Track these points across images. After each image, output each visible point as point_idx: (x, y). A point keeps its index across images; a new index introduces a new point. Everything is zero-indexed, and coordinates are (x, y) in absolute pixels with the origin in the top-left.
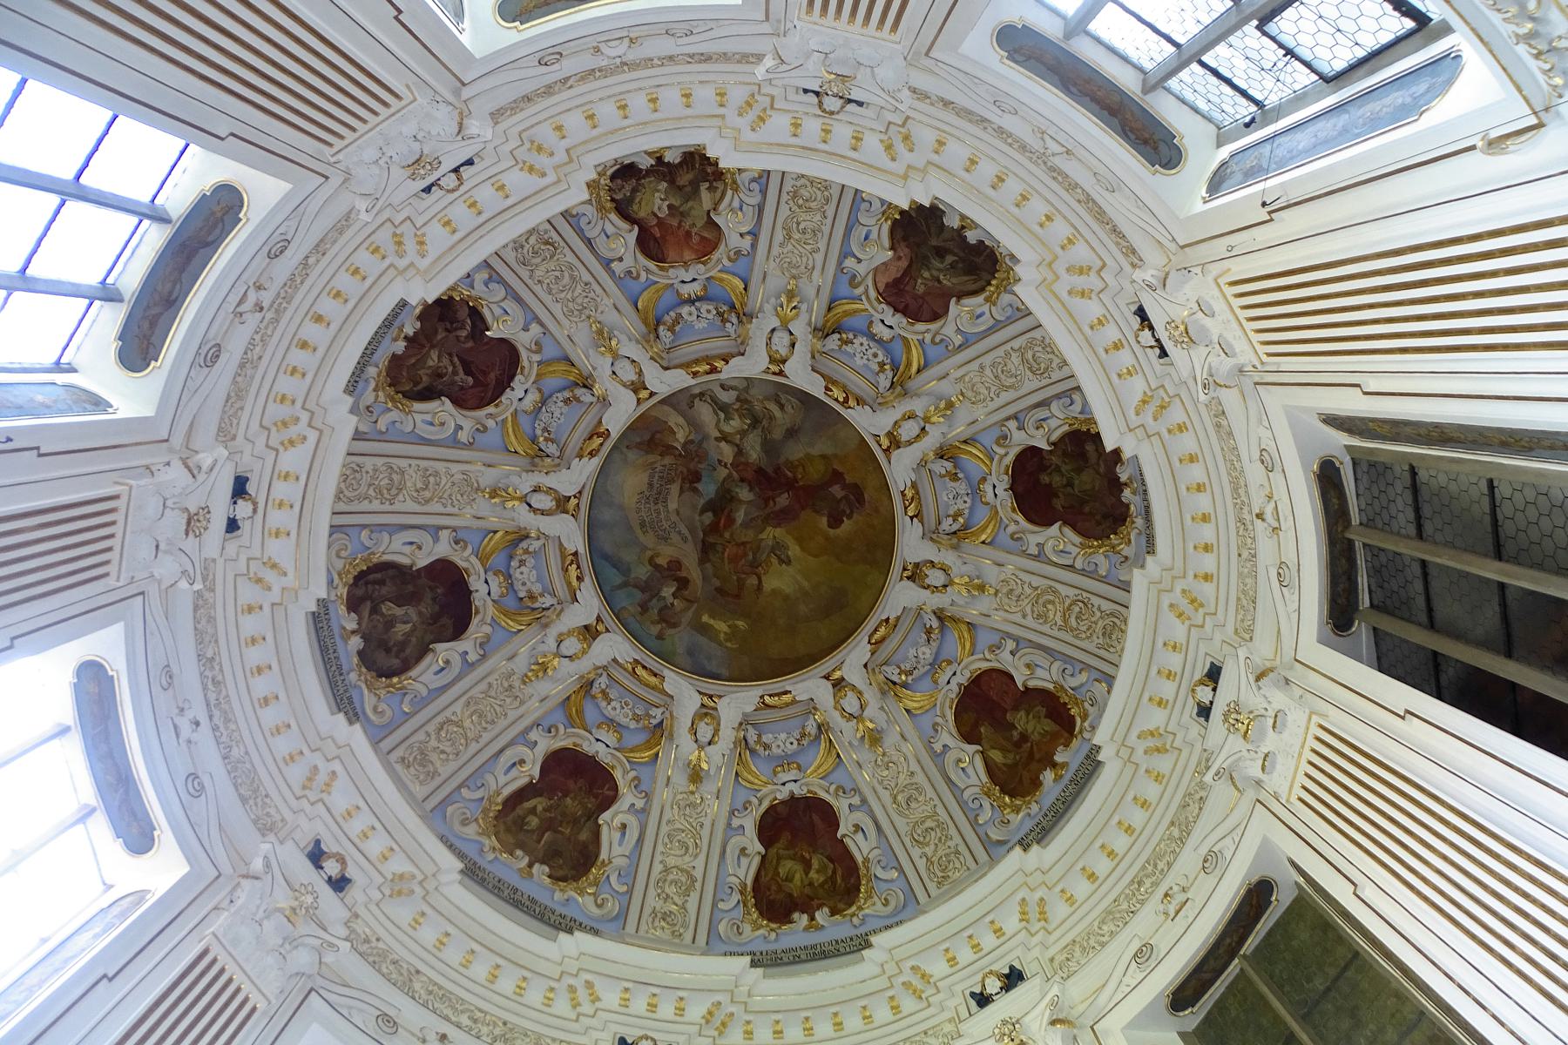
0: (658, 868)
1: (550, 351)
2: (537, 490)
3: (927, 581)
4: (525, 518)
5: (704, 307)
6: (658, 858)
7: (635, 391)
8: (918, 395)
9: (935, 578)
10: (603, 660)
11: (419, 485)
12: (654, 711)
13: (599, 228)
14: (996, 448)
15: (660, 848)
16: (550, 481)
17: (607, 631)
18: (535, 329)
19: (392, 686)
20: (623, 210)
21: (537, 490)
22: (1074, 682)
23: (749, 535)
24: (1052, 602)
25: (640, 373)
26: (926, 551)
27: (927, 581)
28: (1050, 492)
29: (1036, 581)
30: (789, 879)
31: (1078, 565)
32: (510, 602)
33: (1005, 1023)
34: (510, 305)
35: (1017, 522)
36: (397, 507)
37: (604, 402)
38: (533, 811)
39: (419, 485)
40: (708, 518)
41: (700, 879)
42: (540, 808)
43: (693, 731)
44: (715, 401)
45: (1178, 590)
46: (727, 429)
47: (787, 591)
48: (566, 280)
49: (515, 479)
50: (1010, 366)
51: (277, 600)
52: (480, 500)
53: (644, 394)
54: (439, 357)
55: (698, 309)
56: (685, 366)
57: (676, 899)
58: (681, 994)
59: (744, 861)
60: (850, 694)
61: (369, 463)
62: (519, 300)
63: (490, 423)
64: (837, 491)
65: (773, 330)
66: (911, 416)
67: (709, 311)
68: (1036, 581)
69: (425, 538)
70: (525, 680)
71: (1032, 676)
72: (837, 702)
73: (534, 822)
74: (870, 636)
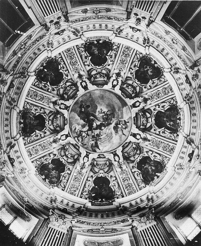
0: (165, 96)
1: (92, 174)
2: (115, 161)
3: (85, 85)
4: (122, 159)
5: (67, 154)
6: (164, 97)
7: (88, 155)
8: (56, 109)
9: (84, 84)
10: (137, 130)
11: (126, 181)
12: (141, 115)
13: (64, 180)
14: (55, 90)
15: (162, 98)
16: (112, 159)
17: (132, 133)
18: (89, 179)
19: (163, 163)
20: (58, 178)
21: (115, 161)
22: (83, 49)
23: (102, 120)
24: (72, 62)
25: (84, 157)
26: (80, 88)
27: (85, 85)
28: (55, 76)
29: (71, 67)
30: (151, 72)
31: (63, 63)
32: (138, 152)
33: (137, 25)
34: (87, 186)
35: (65, 78)
36: (132, 182)
37: (94, 159)
38: (170, 124)
39: (126, 181)
40: (103, 128)
41: (162, 88)
42: (169, 123)
43: (139, 106)
44: (82, 141)
45: (49, 49)
46: (86, 135)
47: (192, 65)
48: (77, 179)
49: (116, 166)
50: (39, 98)
51: (153, 194)
52: (123, 169)
53: (88, 154)
54: (103, 192)
55: (68, 155)
56: (78, 150)
57: (167, 90)
58: (176, 80)
59: (155, 82)
60: (114, 84)
61: (127, 192)
62: (85, 185)
63: (109, 176)
64: (83, 110)
65: (62, 140)
66: (60, 108)
67: (67, 153)
68: (71, 67)
69: (135, 174)
70: (149, 141)
71: (87, 56)
72: (117, 85)
73: (171, 123)
74: (102, 87)
